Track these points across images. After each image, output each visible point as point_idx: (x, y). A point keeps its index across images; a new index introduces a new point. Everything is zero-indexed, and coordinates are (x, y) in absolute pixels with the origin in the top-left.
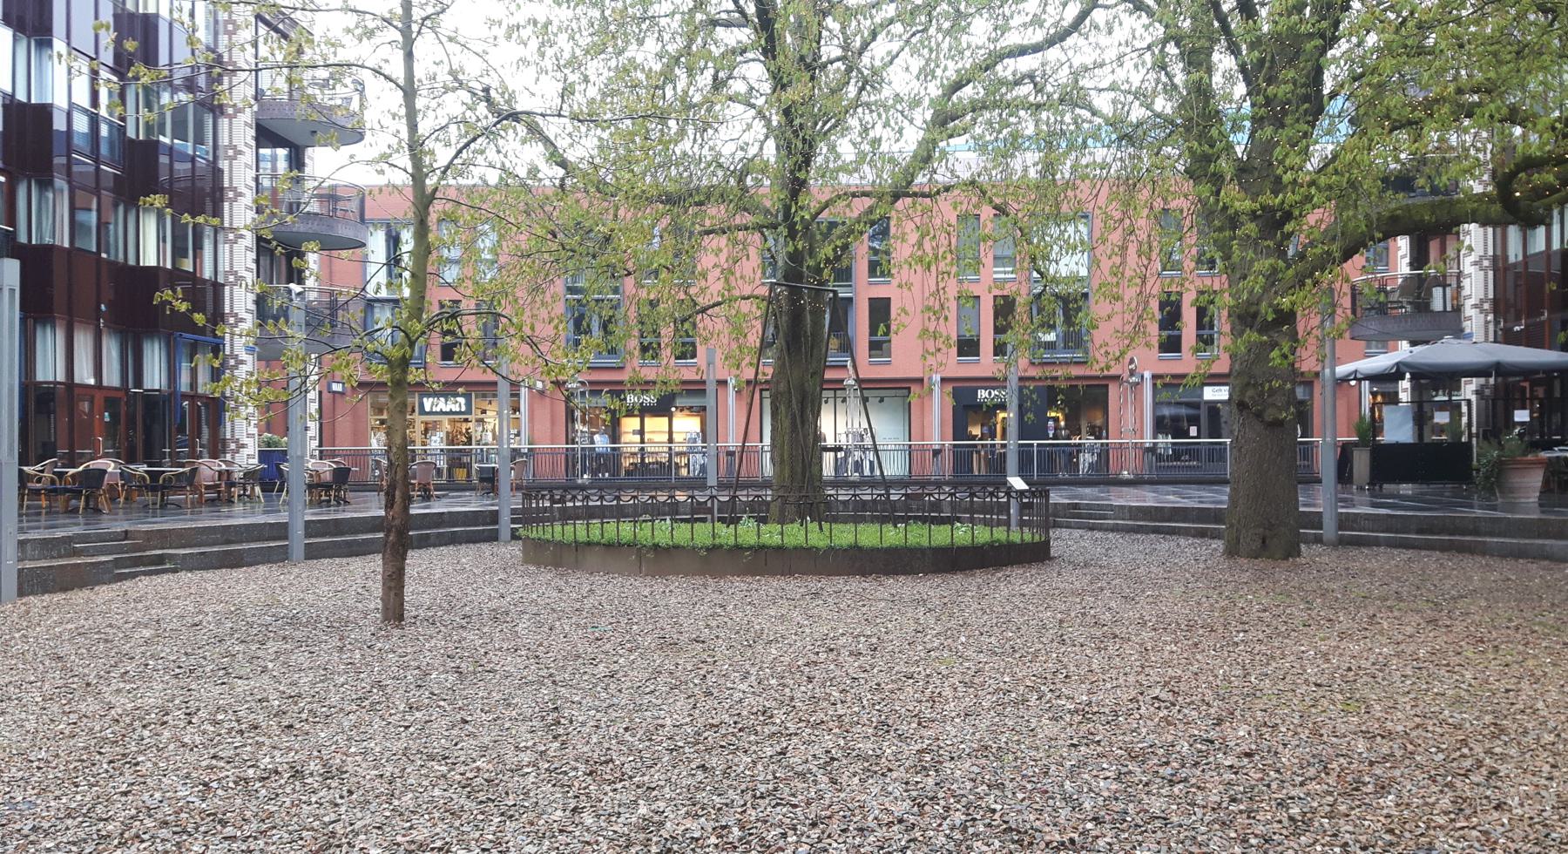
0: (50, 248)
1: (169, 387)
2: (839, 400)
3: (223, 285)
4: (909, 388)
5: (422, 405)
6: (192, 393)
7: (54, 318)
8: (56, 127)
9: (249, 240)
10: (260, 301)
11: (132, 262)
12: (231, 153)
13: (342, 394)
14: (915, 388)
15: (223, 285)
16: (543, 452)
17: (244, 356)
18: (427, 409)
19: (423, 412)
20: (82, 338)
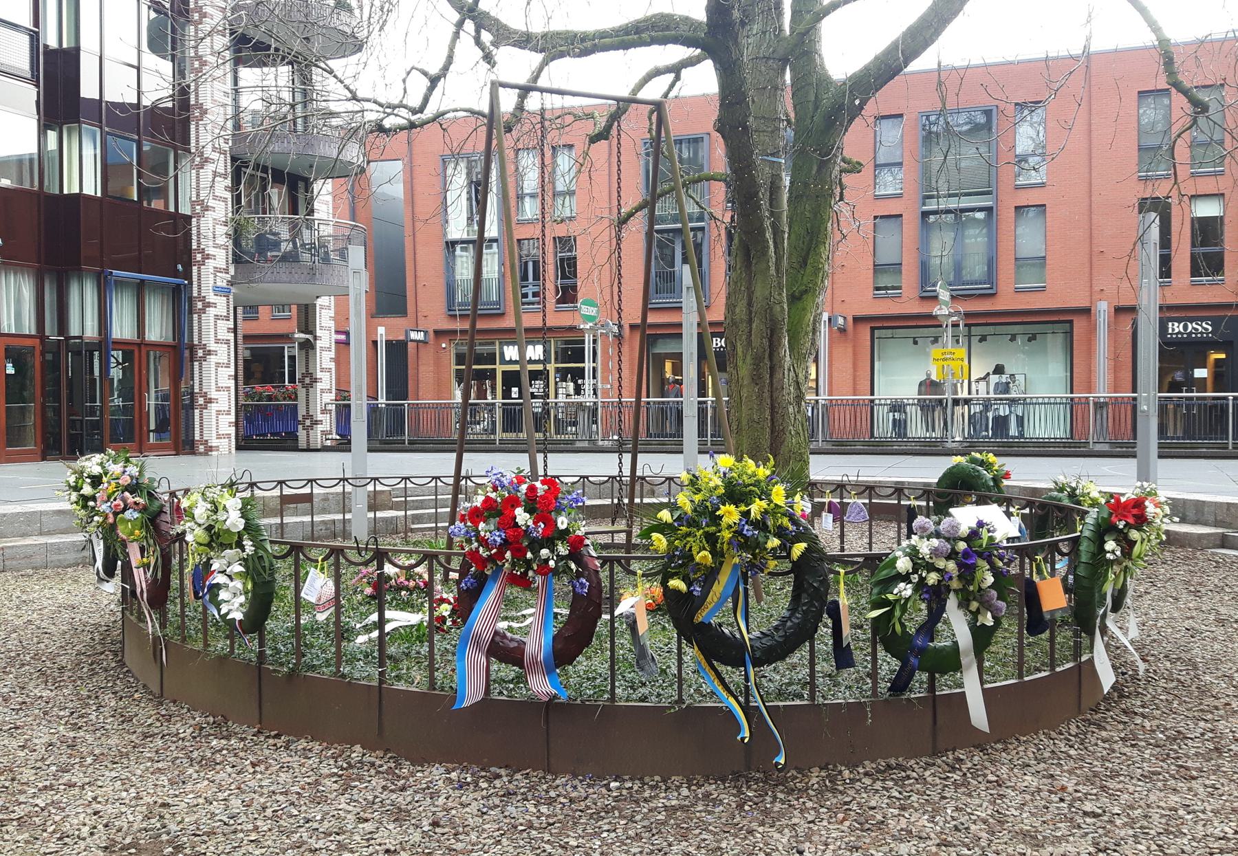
0: (79, 198)
1: (100, 334)
2: (975, 340)
3: (190, 218)
4: (1071, 322)
5: (502, 354)
6: (139, 341)
7: (80, 270)
8: (1196, 370)
9: (222, 164)
10: (237, 236)
11: (172, 209)
12: (196, 64)
13: (425, 342)
14: (1079, 324)
15: (190, 218)
16: (842, 403)
17: (211, 298)
18: (507, 358)
19: (503, 361)
20: (88, 285)
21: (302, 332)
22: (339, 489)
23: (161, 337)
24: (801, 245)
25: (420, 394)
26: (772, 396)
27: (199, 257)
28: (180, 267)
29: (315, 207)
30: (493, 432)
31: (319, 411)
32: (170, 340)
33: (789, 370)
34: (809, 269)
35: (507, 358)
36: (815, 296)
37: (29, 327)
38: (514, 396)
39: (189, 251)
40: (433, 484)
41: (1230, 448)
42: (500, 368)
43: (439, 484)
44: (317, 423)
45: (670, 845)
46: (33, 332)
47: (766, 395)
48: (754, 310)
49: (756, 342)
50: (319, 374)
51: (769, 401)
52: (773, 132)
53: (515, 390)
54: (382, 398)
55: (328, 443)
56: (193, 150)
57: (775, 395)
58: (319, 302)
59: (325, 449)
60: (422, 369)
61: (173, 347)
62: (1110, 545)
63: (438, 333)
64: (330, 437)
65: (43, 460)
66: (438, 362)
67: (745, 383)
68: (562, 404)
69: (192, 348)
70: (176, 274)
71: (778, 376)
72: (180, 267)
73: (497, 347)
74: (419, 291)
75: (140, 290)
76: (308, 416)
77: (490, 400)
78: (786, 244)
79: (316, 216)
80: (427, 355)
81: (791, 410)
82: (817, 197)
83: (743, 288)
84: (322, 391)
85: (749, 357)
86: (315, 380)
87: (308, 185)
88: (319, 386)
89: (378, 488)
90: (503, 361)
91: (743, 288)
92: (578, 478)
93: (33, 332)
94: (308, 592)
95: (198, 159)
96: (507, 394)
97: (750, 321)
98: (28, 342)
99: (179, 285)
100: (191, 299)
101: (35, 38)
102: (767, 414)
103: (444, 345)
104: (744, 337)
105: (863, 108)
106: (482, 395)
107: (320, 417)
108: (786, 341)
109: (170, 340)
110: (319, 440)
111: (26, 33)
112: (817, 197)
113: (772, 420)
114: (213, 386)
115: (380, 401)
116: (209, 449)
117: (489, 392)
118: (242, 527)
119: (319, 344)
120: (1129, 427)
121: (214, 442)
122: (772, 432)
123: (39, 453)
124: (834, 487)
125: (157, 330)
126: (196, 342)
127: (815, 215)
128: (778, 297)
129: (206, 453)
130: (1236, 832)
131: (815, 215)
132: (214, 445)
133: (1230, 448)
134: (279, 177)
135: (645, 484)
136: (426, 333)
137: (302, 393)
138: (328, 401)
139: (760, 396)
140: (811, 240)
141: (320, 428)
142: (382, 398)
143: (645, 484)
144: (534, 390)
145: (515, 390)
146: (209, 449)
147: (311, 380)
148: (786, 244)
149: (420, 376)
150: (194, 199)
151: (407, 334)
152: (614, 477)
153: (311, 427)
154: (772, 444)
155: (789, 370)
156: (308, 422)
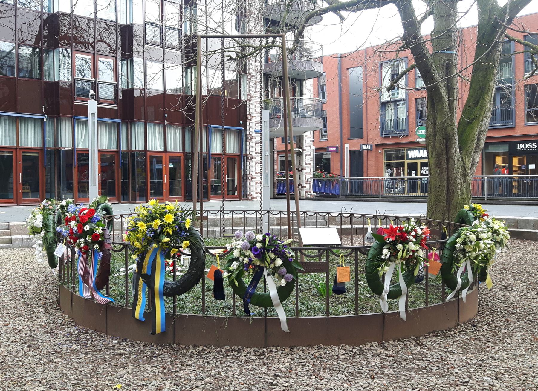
1: (207, 151)
5: (407, 155)
13: (371, 150)
17: (254, 135)
19: (408, 158)
21: (298, 148)
22: (279, 216)
23: (234, 152)
24: (476, 95)
25: (369, 174)
26: (448, 174)
27: (249, 118)
28: (241, 122)
29: (304, 92)
30: (403, 192)
31: (304, 182)
32: (237, 153)
33: (458, 160)
34: (479, 107)
35: (410, 157)
36: (479, 121)
37: (179, 149)
38: (413, 175)
39: (245, 115)
40: (327, 215)
41: (486, 200)
42: (406, 162)
43: (318, 215)
44: (303, 187)
45: (78, 367)
46: (181, 151)
47: (444, 173)
48: (436, 129)
49: (438, 146)
50: (304, 166)
51: (446, 177)
52: (447, 38)
53: (414, 172)
54: (347, 176)
55: (309, 196)
56: (247, 73)
57: (450, 173)
58: (305, 134)
59: (307, 199)
60: (369, 163)
61: (239, 156)
62: (385, 251)
63: (377, 146)
64: (309, 194)
65: (184, 201)
66: (377, 160)
67: (432, 167)
68: (348, 180)
69: (247, 156)
70: (239, 125)
71: (451, 163)
72: (241, 122)
73: (405, 152)
74: (368, 126)
75: (223, 133)
76: (300, 184)
77: (402, 176)
78: (43, 109)
79: (304, 96)
80: (372, 156)
81: (459, 181)
82: (486, 69)
83: (431, 119)
84: (306, 173)
85: (434, 154)
86: (303, 169)
87: (301, 82)
88: (304, 171)
89: (282, 216)
90: (408, 158)
91: (431, 119)
92: (349, 215)
93: (181, 151)
94: (57, 252)
95: (249, 76)
96: (410, 174)
97: (435, 136)
98: (179, 155)
99: (241, 130)
100: (246, 135)
101: (180, 32)
102: (445, 183)
103: (380, 151)
104: (432, 144)
105: (512, 21)
106: (398, 174)
107: (305, 185)
108: (457, 145)
109: (237, 153)
110: (304, 195)
111: (177, 30)
112: (486, 69)
113: (448, 186)
114: (254, 172)
115: (346, 177)
116: (253, 198)
117: (402, 173)
118: (41, 226)
119: (304, 153)
120: (480, 188)
121: (254, 195)
122: (448, 193)
123: (183, 199)
124: (394, 218)
125: (232, 148)
126: (248, 154)
127: (485, 79)
128: (450, 123)
129: (251, 200)
130: (187, 390)
131: (485, 79)
132: (254, 196)
133: (486, 200)
134: (297, 80)
135: (353, 217)
136: (371, 146)
137: (297, 174)
138: (309, 178)
139: (440, 174)
140: (482, 92)
141: (305, 190)
142: (347, 176)
143: (353, 217)
144: (423, 172)
145: (414, 172)
146: (253, 198)
147: (300, 169)
148: (43, 109)
149: (369, 166)
150: (248, 93)
151: (361, 146)
152: (221, 211)
153: (301, 189)
154: (447, 199)
155: (458, 160)
156: (300, 187)
